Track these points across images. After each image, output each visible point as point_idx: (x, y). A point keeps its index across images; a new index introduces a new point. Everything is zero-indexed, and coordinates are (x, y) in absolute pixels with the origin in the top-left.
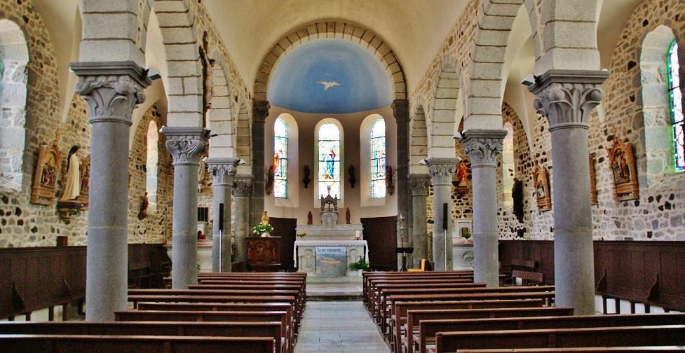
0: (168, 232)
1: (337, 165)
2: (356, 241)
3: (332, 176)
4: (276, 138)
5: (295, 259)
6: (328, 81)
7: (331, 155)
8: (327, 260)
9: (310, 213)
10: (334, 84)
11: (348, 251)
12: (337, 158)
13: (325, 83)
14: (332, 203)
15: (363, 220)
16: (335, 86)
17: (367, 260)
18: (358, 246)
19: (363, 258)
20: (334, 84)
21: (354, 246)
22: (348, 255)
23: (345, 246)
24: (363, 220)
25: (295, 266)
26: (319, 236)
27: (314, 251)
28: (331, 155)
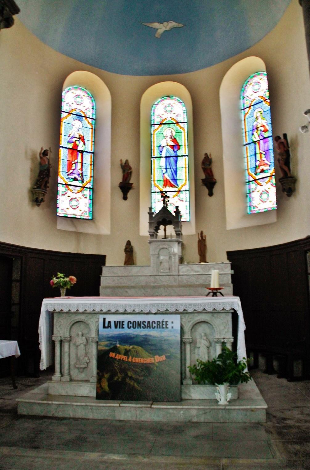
0: (118, 291)
1: (183, 163)
2: (211, 300)
3: (175, 180)
4: (63, 115)
5: (44, 347)
6: (161, 22)
7: (172, 146)
8: (127, 353)
9: (129, 243)
10: (172, 24)
11: (187, 328)
12: (183, 151)
13: (156, 25)
14: (170, 223)
15: (231, 255)
16: (173, 28)
17: (242, 352)
18: (215, 312)
19: (229, 346)
20: (172, 24)
21: (204, 311)
22: (187, 336)
23: (176, 313)
24: (231, 255)
25: (44, 365)
26: (143, 287)
27: (93, 328)
28: (172, 146)
